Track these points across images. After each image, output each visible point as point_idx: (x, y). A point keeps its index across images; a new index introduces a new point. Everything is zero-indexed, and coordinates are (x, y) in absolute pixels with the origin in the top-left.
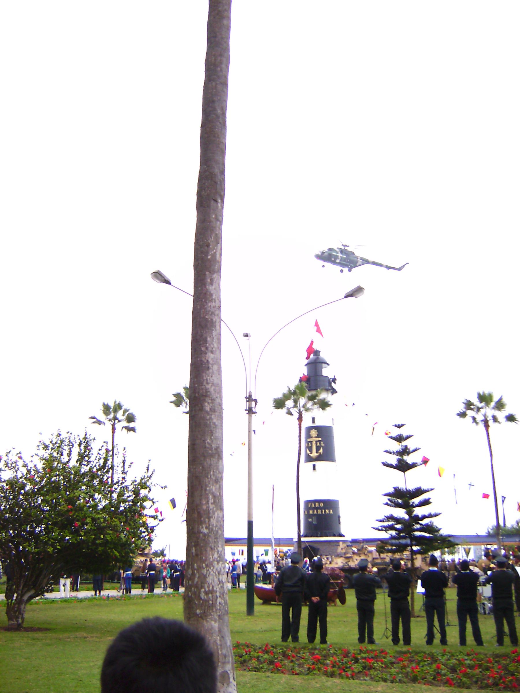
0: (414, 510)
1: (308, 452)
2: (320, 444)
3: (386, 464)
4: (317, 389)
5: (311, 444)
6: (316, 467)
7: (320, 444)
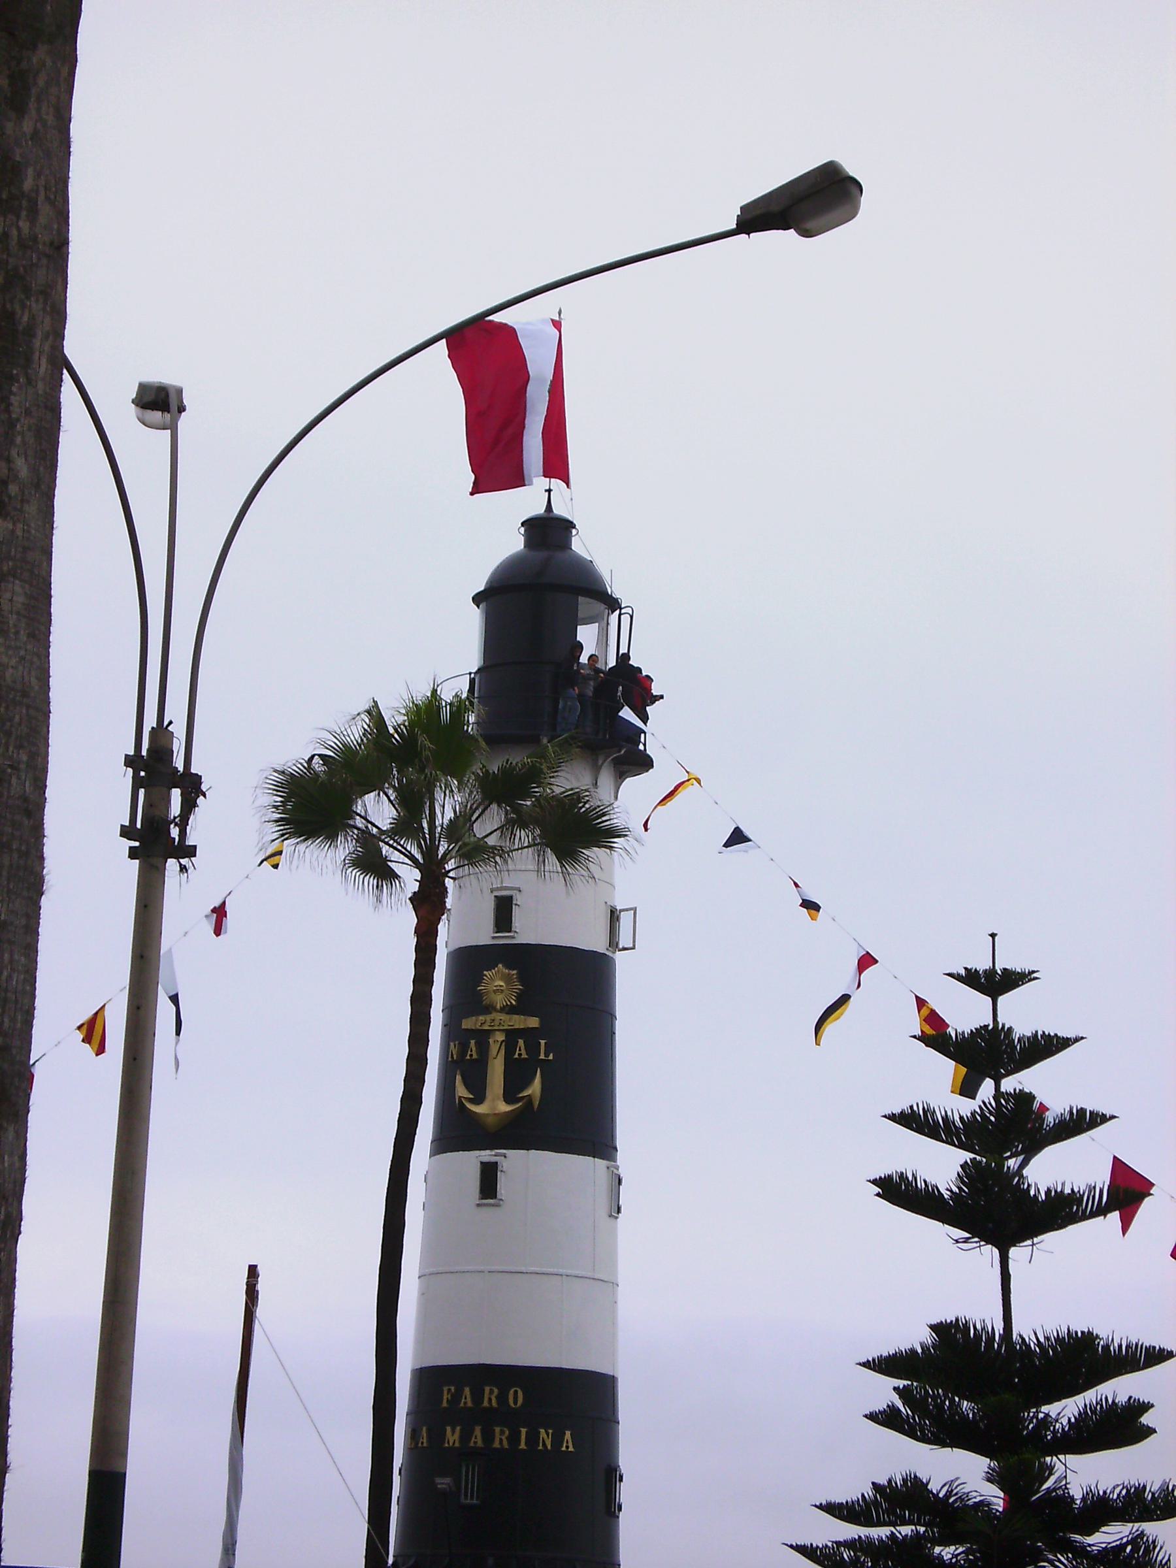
0: (1051, 1469)
1: (461, 1091)
2: (533, 1048)
3: (899, 1191)
4: (536, 740)
5: (483, 1048)
7: (533, 1048)
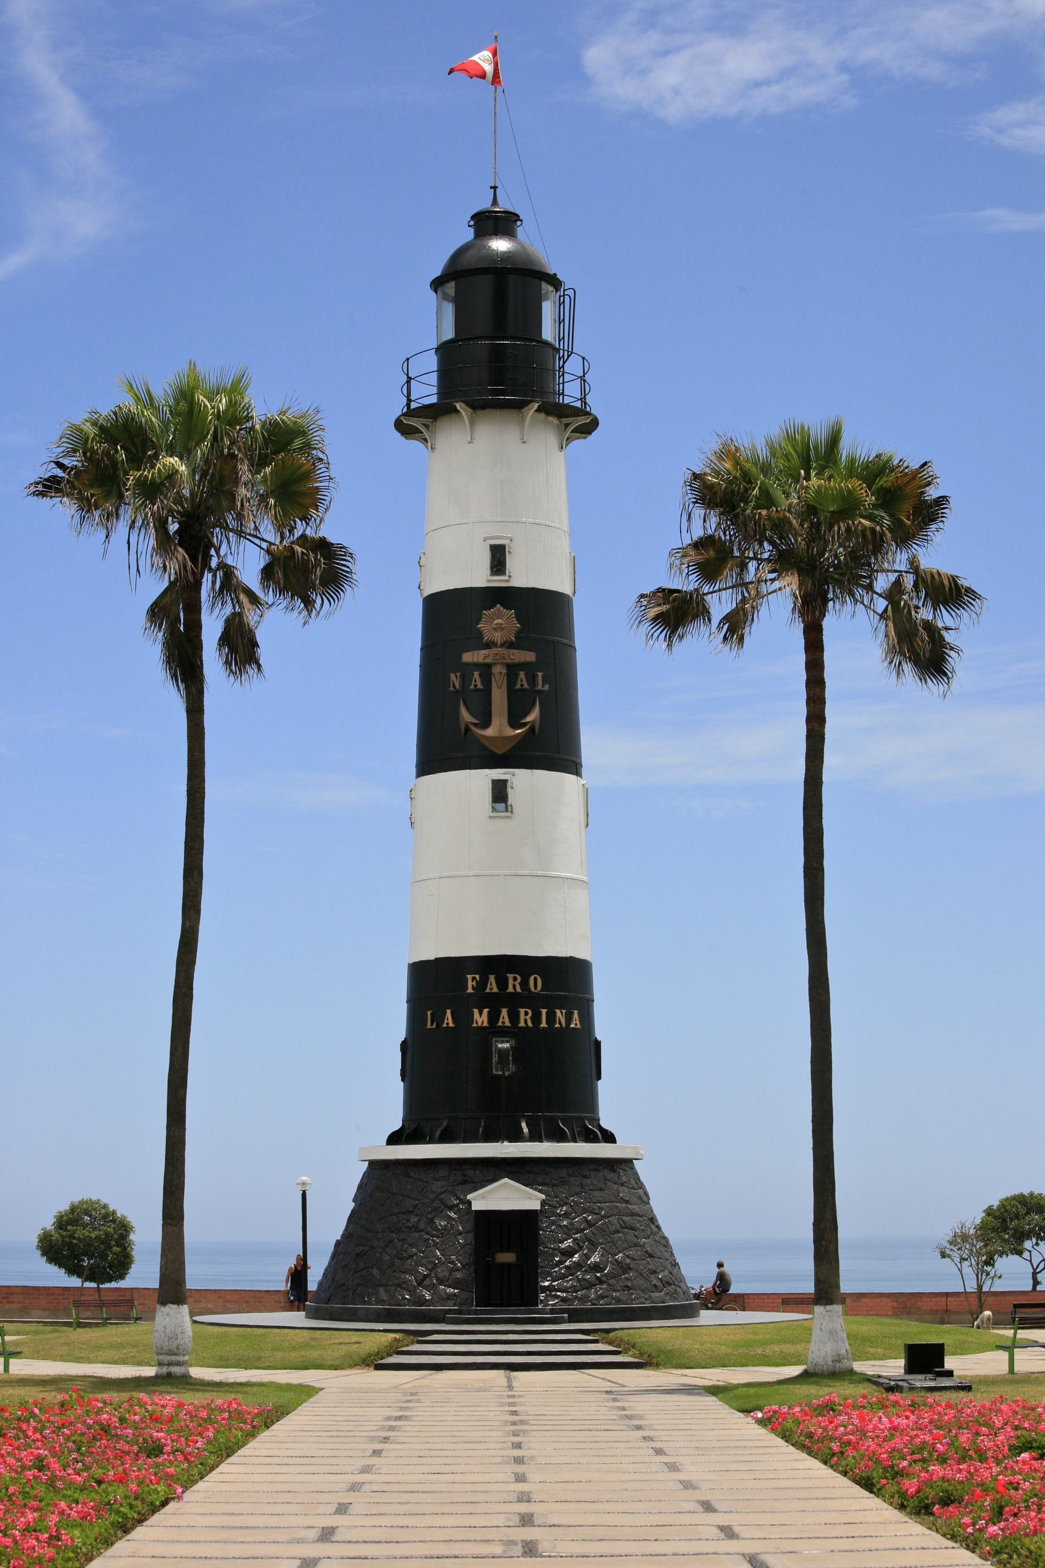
6: (513, 796)
7: (532, 679)
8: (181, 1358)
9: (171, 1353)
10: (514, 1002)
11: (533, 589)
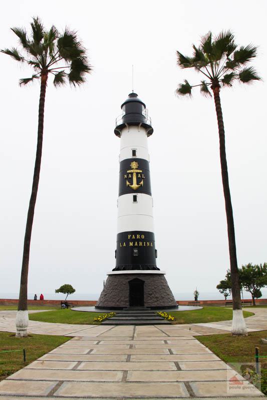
2: (141, 176)
7: (141, 176)
8: (24, 329)
9: (20, 327)
10: (138, 241)
11: (140, 159)
